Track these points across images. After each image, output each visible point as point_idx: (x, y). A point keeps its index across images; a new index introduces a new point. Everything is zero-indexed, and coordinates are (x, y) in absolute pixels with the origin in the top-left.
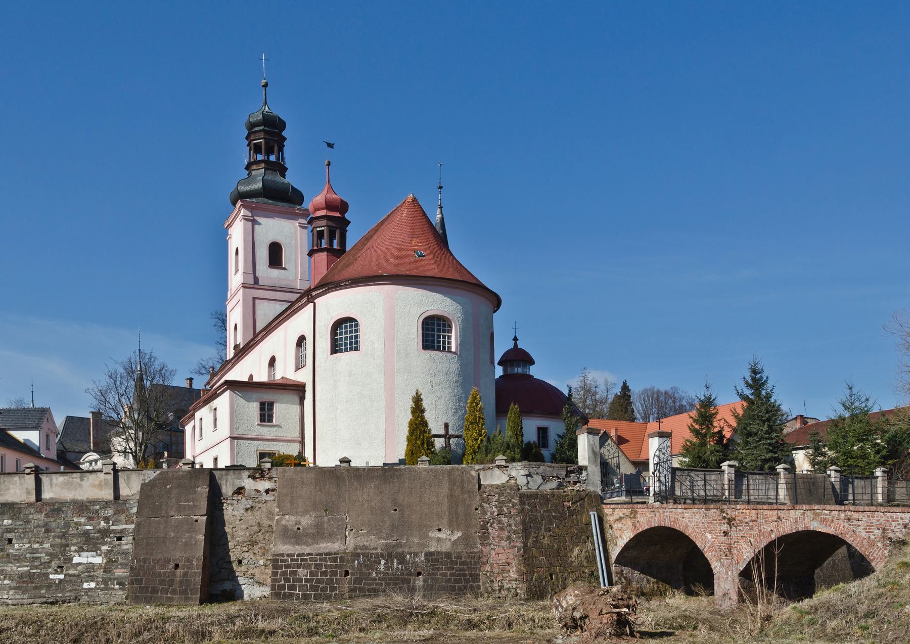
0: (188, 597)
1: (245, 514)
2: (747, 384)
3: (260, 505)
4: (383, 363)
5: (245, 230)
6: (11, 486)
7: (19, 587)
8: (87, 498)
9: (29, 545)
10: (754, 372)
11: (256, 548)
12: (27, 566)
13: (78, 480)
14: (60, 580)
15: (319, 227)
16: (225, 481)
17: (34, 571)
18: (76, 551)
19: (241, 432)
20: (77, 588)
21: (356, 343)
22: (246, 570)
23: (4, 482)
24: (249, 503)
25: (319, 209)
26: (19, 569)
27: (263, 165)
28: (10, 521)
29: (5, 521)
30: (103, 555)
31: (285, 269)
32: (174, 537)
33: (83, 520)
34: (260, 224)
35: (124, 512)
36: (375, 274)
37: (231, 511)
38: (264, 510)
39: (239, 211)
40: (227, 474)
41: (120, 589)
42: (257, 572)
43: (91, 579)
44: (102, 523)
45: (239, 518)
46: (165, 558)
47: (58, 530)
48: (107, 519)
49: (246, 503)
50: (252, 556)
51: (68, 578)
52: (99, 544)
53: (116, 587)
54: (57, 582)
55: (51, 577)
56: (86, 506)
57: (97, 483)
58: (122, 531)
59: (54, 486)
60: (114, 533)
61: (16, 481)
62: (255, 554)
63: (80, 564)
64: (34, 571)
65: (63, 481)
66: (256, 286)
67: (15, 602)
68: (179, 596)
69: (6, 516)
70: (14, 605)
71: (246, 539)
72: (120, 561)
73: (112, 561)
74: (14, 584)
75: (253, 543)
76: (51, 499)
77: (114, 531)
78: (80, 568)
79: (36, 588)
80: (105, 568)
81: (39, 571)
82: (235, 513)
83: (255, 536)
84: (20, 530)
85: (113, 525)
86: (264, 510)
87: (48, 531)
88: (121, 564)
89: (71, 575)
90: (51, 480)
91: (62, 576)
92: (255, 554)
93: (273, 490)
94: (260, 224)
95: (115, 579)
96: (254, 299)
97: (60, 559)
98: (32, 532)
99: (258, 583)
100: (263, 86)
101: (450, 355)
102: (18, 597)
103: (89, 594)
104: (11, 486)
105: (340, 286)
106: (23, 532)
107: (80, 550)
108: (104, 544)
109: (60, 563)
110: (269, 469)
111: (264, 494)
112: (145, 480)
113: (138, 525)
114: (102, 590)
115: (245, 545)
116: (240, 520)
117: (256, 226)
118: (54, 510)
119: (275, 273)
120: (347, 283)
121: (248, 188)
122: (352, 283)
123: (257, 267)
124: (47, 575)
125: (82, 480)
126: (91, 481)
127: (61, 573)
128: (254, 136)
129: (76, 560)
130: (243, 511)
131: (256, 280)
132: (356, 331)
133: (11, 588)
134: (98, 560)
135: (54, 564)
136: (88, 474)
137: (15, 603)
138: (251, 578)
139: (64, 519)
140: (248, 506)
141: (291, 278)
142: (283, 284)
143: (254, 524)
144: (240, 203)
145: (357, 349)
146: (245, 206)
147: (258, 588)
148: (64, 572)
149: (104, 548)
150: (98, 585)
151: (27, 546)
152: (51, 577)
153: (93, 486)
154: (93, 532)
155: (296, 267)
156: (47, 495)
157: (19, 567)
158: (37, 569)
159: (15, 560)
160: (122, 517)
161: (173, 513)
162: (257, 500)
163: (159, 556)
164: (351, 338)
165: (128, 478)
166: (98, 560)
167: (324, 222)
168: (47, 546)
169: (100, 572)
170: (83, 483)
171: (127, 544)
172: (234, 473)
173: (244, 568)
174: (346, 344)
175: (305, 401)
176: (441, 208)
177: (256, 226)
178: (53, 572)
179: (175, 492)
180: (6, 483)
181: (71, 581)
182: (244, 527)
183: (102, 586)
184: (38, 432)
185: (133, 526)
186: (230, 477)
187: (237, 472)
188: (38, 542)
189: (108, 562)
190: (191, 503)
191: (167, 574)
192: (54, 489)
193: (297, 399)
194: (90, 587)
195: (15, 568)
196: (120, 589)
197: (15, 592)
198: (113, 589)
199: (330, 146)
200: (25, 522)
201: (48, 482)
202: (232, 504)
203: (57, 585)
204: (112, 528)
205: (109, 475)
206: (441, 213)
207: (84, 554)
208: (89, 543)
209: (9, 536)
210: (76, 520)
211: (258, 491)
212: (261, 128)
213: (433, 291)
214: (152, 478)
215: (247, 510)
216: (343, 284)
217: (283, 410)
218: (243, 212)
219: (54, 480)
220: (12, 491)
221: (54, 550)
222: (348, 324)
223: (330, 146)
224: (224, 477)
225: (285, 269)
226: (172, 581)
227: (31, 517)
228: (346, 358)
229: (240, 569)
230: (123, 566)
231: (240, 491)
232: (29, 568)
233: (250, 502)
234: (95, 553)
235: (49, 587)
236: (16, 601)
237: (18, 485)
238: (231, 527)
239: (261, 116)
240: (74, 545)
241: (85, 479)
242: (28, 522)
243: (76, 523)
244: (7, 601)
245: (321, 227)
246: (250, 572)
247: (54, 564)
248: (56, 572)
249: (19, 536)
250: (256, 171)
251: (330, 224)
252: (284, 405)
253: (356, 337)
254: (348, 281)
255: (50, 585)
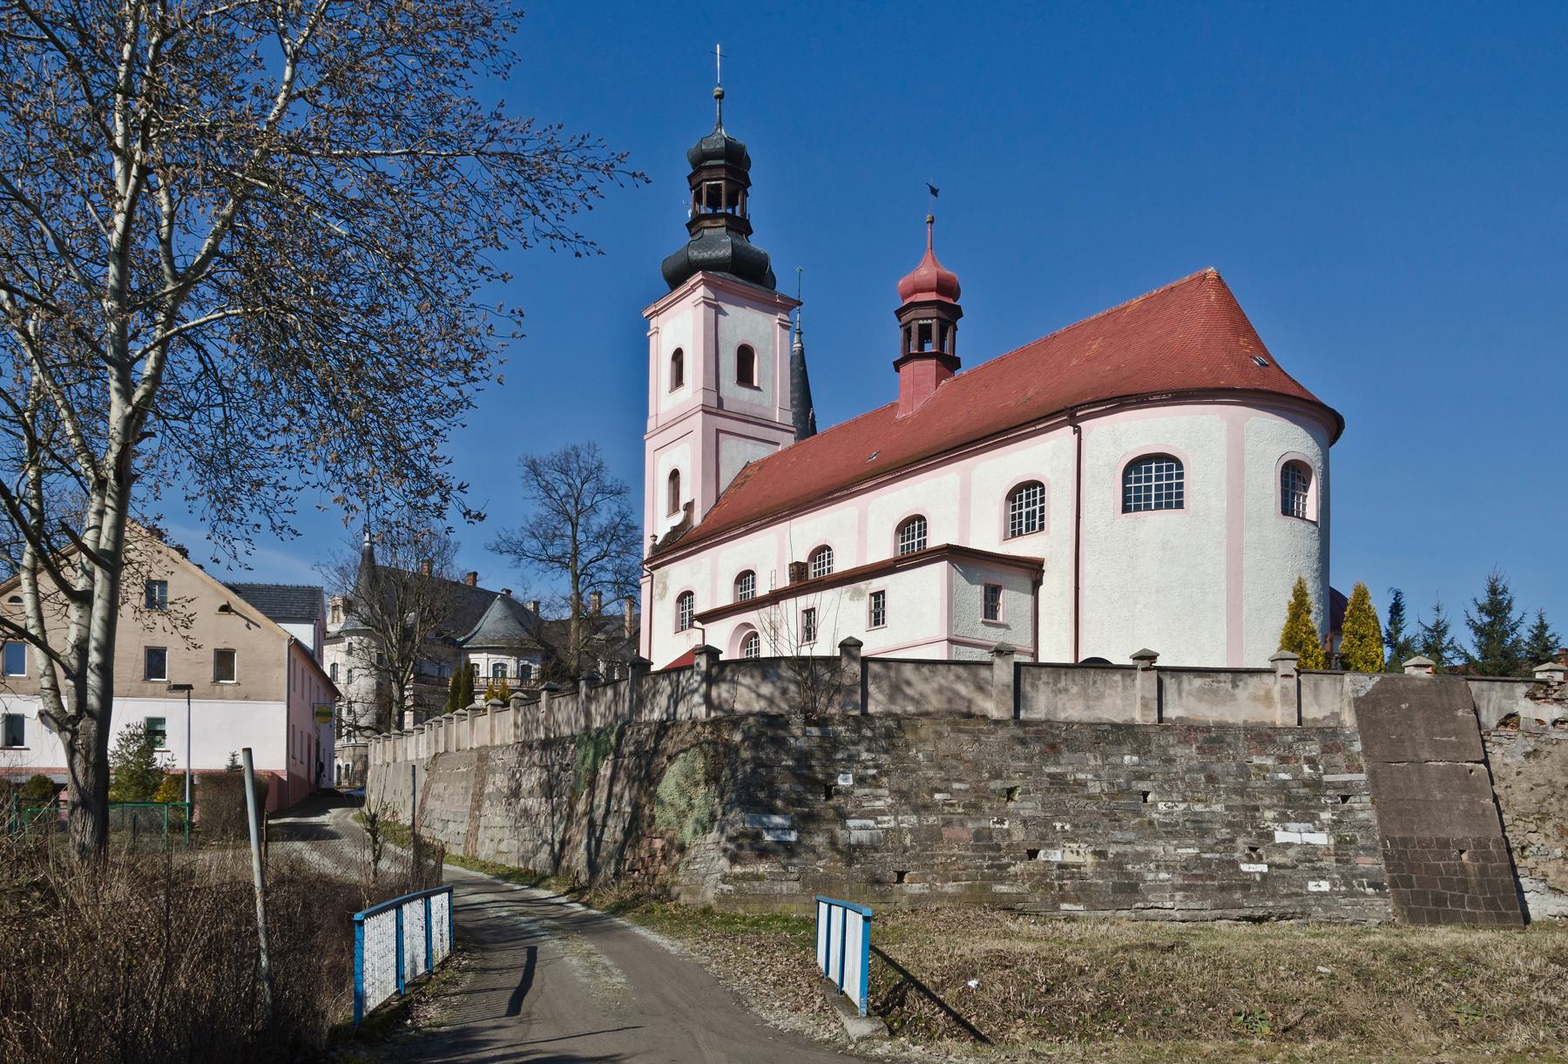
0: (1502, 914)
1: (1526, 764)
2: (1481, 609)
3: (1549, 748)
4: (1225, 532)
5: (706, 320)
6: (1108, 692)
7: (1190, 885)
8: (1245, 721)
9: (1185, 805)
10: (1493, 591)
11: (1549, 825)
12: (1192, 846)
13: (1229, 686)
14: (1264, 876)
15: (923, 319)
16: (1485, 702)
17: (1208, 856)
18: (1275, 820)
19: (959, 633)
20: (1299, 891)
21: (1180, 495)
22: (1534, 865)
23: (1095, 682)
24: (1531, 744)
25: (922, 291)
26: (1179, 851)
27: (723, 222)
28: (1135, 759)
29: (1127, 758)
30: (1327, 830)
31: (758, 388)
32: (1442, 801)
33: (1270, 762)
34: (725, 314)
35: (1339, 750)
36: (1216, 386)
37: (1499, 755)
38: (1556, 756)
39: (693, 289)
40: (1490, 689)
41: (1377, 894)
42: (1551, 869)
43: (1320, 874)
44: (1306, 769)
45: (1515, 770)
46: (1437, 839)
47: (1231, 779)
48: (1312, 762)
49: (1525, 743)
50: (1543, 840)
51: (1275, 872)
52: (1315, 808)
53: (1370, 891)
54: (1258, 878)
55: (1244, 867)
56: (1269, 736)
57: (1262, 693)
58: (1345, 784)
59: (1184, 695)
60: (1335, 788)
61: (1116, 682)
62: (1547, 836)
63: (1289, 845)
64: (1208, 856)
65: (1200, 687)
66: (721, 412)
67: (1187, 915)
68: (1484, 911)
69: (1125, 749)
70: (1184, 921)
71: (1532, 807)
72: (1361, 842)
73: (1346, 842)
74: (1179, 881)
75: (1544, 817)
76: (1180, 719)
77: (1332, 785)
78: (1291, 852)
79: (1222, 888)
80: (1336, 854)
81: (1218, 856)
82: (1508, 760)
83: (1545, 804)
84: (1160, 777)
85: (1325, 773)
86: (1556, 756)
87: (1211, 779)
88: (1363, 848)
89: (1279, 866)
90: (1180, 684)
91: (1264, 868)
92: (1547, 836)
93: (1562, 723)
94: (725, 314)
95: (1362, 876)
96: (718, 431)
97: (1249, 834)
98: (1183, 779)
99: (1553, 889)
100: (717, 97)
101: (1303, 525)
102: (1192, 905)
103: (1324, 902)
104: (1108, 692)
105: (1148, 401)
106: (1166, 781)
107: (1283, 819)
108: (1324, 808)
109: (1252, 840)
110: (1560, 683)
111: (1551, 728)
112: (1357, 691)
113: (1372, 774)
114: (1345, 896)
115: (1531, 818)
116: (1519, 773)
117: (721, 317)
118: (1211, 741)
119: (745, 393)
120: (1164, 397)
121: (706, 255)
122: (1173, 398)
123: (721, 381)
124: (1234, 864)
125: (1235, 686)
126: (1251, 689)
127: (1260, 860)
129: (1280, 837)
130: (1521, 758)
131: (720, 401)
132: (1180, 476)
133: (1176, 888)
134: (1321, 839)
135: (1242, 842)
136: (1245, 676)
137: (1187, 918)
138: (1542, 881)
139: (1234, 759)
140: (1530, 749)
141: (766, 404)
142: (757, 412)
143: (1542, 782)
144: (700, 277)
145: (1180, 505)
146: (706, 283)
147: (1552, 899)
148: (1265, 860)
149: (1326, 816)
150: (1335, 886)
151: (1182, 806)
152: (1244, 867)
153: (1255, 698)
154: (1294, 784)
155: (774, 387)
156: (1171, 712)
157: (1177, 847)
158: (1213, 851)
159: (1167, 833)
160: (1339, 759)
161: (1428, 756)
162: (1543, 739)
163: (1427, 834)
164: (1169, 486)
165: (1316, 686)
166: (1321, 839)
167: (932, 312)
168: (1218, 808)
169: (1329, 862)
170: (1237, 691)
171: (1363, 809)
172: (1502, 688)
173: (1530, 862)
174: (1148, 498)
175: (1041, 588)
176: (800, 333)
177: (721, 317)
178: (1245, 859)
179: (1419, 717)
180: (1098, 685)
181: (1284, 877)
182: (1525, 786)
183: (1343, 889)
184: (312, 626)
185: (1363, 776)
186: (1494, 695)
187: (1507, 685)
188: (1199, 801)
189: (1339, 842)
190: (1453, 738)
191: (1452, 870)
192: (1184, 700)
193: (1029, 586)
194: (1322, 889)
195: (1172, 848)
196: (1377, 894)
197: (1186, 896)
198: (1365, 895)
199: (934, 192)
200: (1164, 761)
201: (1175, 687)
202: (1500, 744)
203: (1259, 885)
204: (1327, 778)
205: (1289, 679)
206: (800, 342)
207: (1292, 826)
208: (1299, 805)
209: (1143, 786)
210: (1256, 760)
211: (1540, 722)
212: (722, 162)
213: (1295, 422)
214: (1369, 688)
215: (1527, 755)
216: (1155, 398)
217: (1012, 602)
218: (701, 291)
219: (1185, 685)
220: (1108, 701)
221: (1234, 817)
222: (1154, 465)
223: (934, 192)
224: (1485, 694)
225: (758, 388)
226: (1465, 882)
227: (1172, 751)
228: (1154, 521)
229: (1524, 863)
230: (1370, 850)
231: (1510, 720)
232: (1197, 851)
233: (1532, 741)
234: (1311, 825)
235: (1245, 887)
236: (1190, 913)
237: (1119, 689)
238: (1503, 785)
239: (723, 144)
240: (1269, 808)
241: (1241, 684)
242: (1170, 761)
243: (1259, 767)
244: (1172, 912)
245: (927, 319)
246: (1541, 868)
247: (1242, 842)
248: (1251, 860)
249: (1161, 786)
250: (712, 231)
251: (941, 315)
252: (1013, 593)
253: (1180, 486)
254: (1167, 394)
255: (1246, 885)
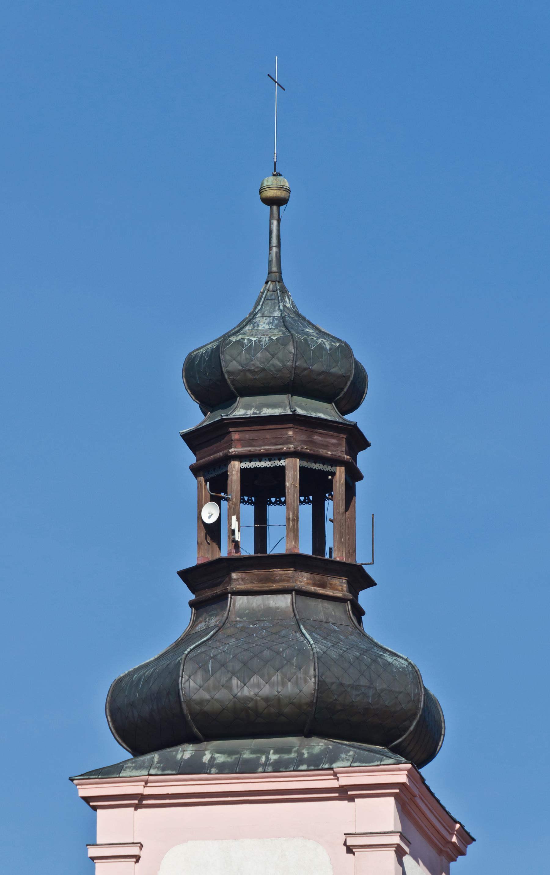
128: (304, 437)
144: (402, 778)
